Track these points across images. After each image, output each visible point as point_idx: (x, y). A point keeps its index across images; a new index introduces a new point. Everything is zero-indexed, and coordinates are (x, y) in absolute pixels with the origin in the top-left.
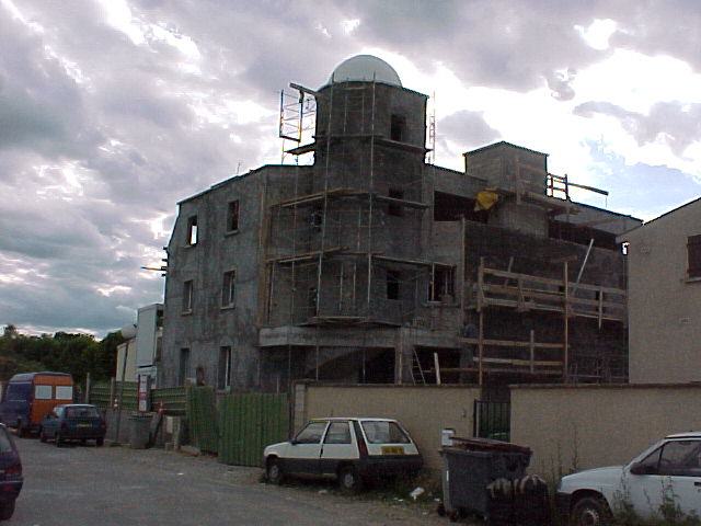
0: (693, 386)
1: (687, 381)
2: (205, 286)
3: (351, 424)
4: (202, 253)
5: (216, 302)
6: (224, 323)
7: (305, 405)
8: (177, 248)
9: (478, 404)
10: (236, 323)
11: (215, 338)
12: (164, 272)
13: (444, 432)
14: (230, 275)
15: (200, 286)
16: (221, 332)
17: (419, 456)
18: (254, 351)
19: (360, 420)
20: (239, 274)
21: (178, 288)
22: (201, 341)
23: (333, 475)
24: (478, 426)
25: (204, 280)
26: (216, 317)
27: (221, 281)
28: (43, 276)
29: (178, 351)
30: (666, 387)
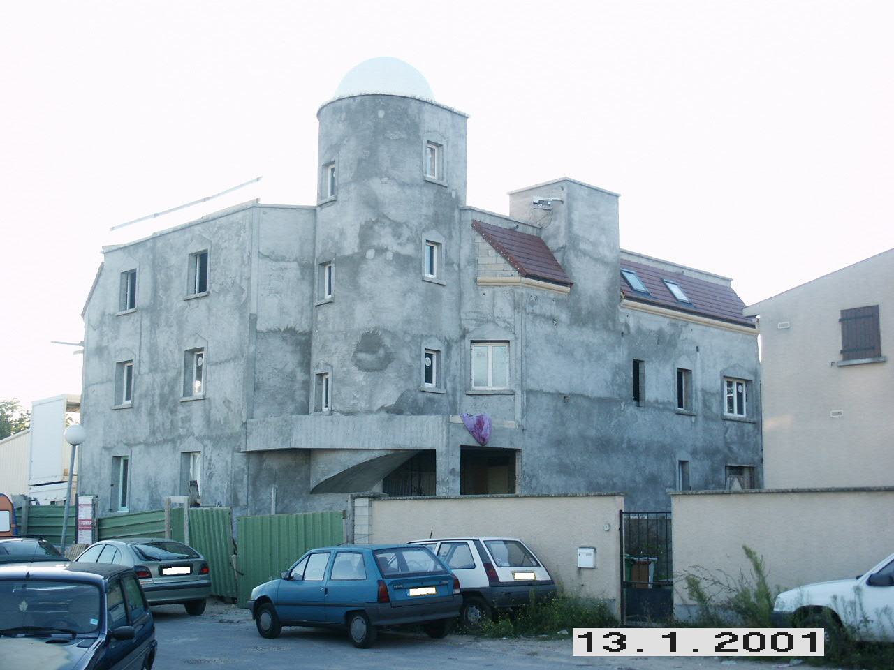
0: (889, 490)
1: (880, 484)
2: (154, 370)
3: (471, 544)
4: (146, 322)
5: (172, 392)
6: (187, 420)
7: (370, 525)
8: (103, 315)
9: (624, 517)
10: (208, 420)
11: (173, 441)
12: (82, 348)
13: (580, 550)
14: (196, 352)
15: (145, 369)
16: (182, 432)
17: (552, 582)
18: (238, 456)
19: (481, 540)
20: (211, 351)
21: (106, 369)
22: (147, 445)
23: (458, 614)
24: (297, 562)
25: (152, 360)
26: (173, 412)
27: (179, 359)
28: (661, 355)
29: (108, 460)
30: (810, 491)
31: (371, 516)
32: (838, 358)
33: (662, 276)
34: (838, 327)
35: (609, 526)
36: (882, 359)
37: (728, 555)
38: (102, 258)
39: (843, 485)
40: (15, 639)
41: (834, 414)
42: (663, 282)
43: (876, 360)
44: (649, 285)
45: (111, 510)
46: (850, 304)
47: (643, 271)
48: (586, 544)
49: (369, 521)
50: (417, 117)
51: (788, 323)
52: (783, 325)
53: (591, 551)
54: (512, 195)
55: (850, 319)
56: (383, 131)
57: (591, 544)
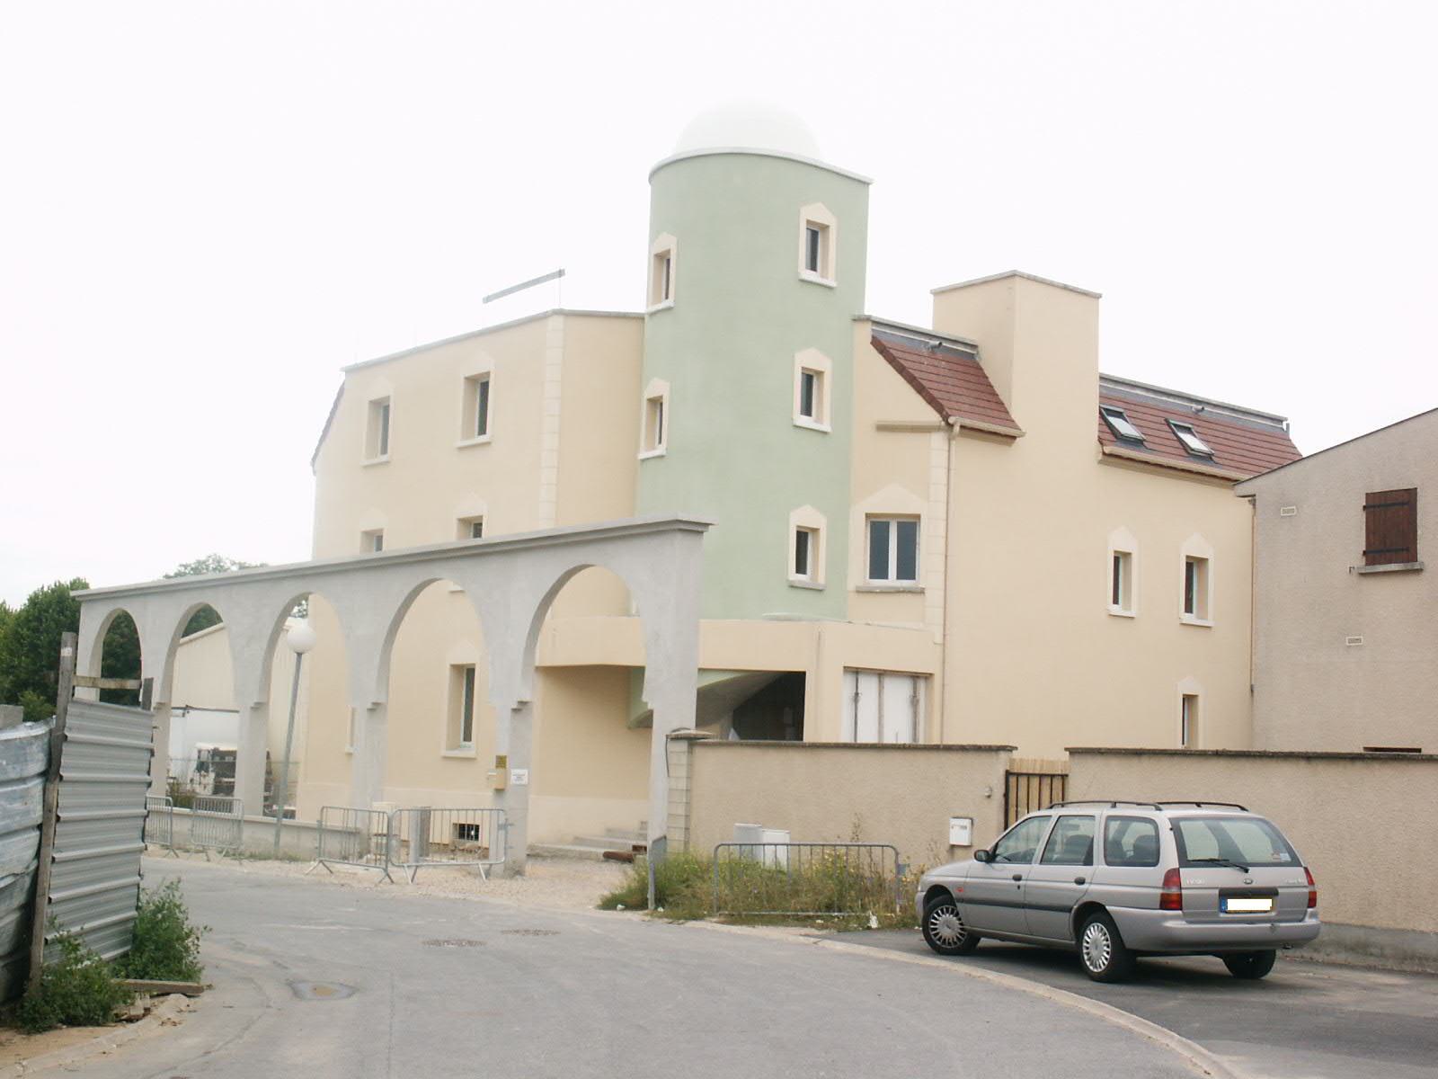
7: (689, 778)
13: (954, 822)
31: (691, 765)
32: (1359, 561)
33: (1166, 415)
34: (1361, 518)
35: (991, 790)
36: (1417, 566)
37: (987, 794)
38: (343, 377)
39: (291, 679)
40: (105, 1028)
41: (1351, 641)
42: (1168, 424)
43: (1409, 566)
44: (1145, 430)
45: (53, 859)
46: (1378, 488)
47: (1138, 408)
48: (961, 813)
49: (688, 772)
50: (486, 890)
51: (1294, 507)
52: (1289, 511)
53: (967, 822)
54: (938, 293)
55: (1379, 506)
56: (750, 215)
57: (970, 816)
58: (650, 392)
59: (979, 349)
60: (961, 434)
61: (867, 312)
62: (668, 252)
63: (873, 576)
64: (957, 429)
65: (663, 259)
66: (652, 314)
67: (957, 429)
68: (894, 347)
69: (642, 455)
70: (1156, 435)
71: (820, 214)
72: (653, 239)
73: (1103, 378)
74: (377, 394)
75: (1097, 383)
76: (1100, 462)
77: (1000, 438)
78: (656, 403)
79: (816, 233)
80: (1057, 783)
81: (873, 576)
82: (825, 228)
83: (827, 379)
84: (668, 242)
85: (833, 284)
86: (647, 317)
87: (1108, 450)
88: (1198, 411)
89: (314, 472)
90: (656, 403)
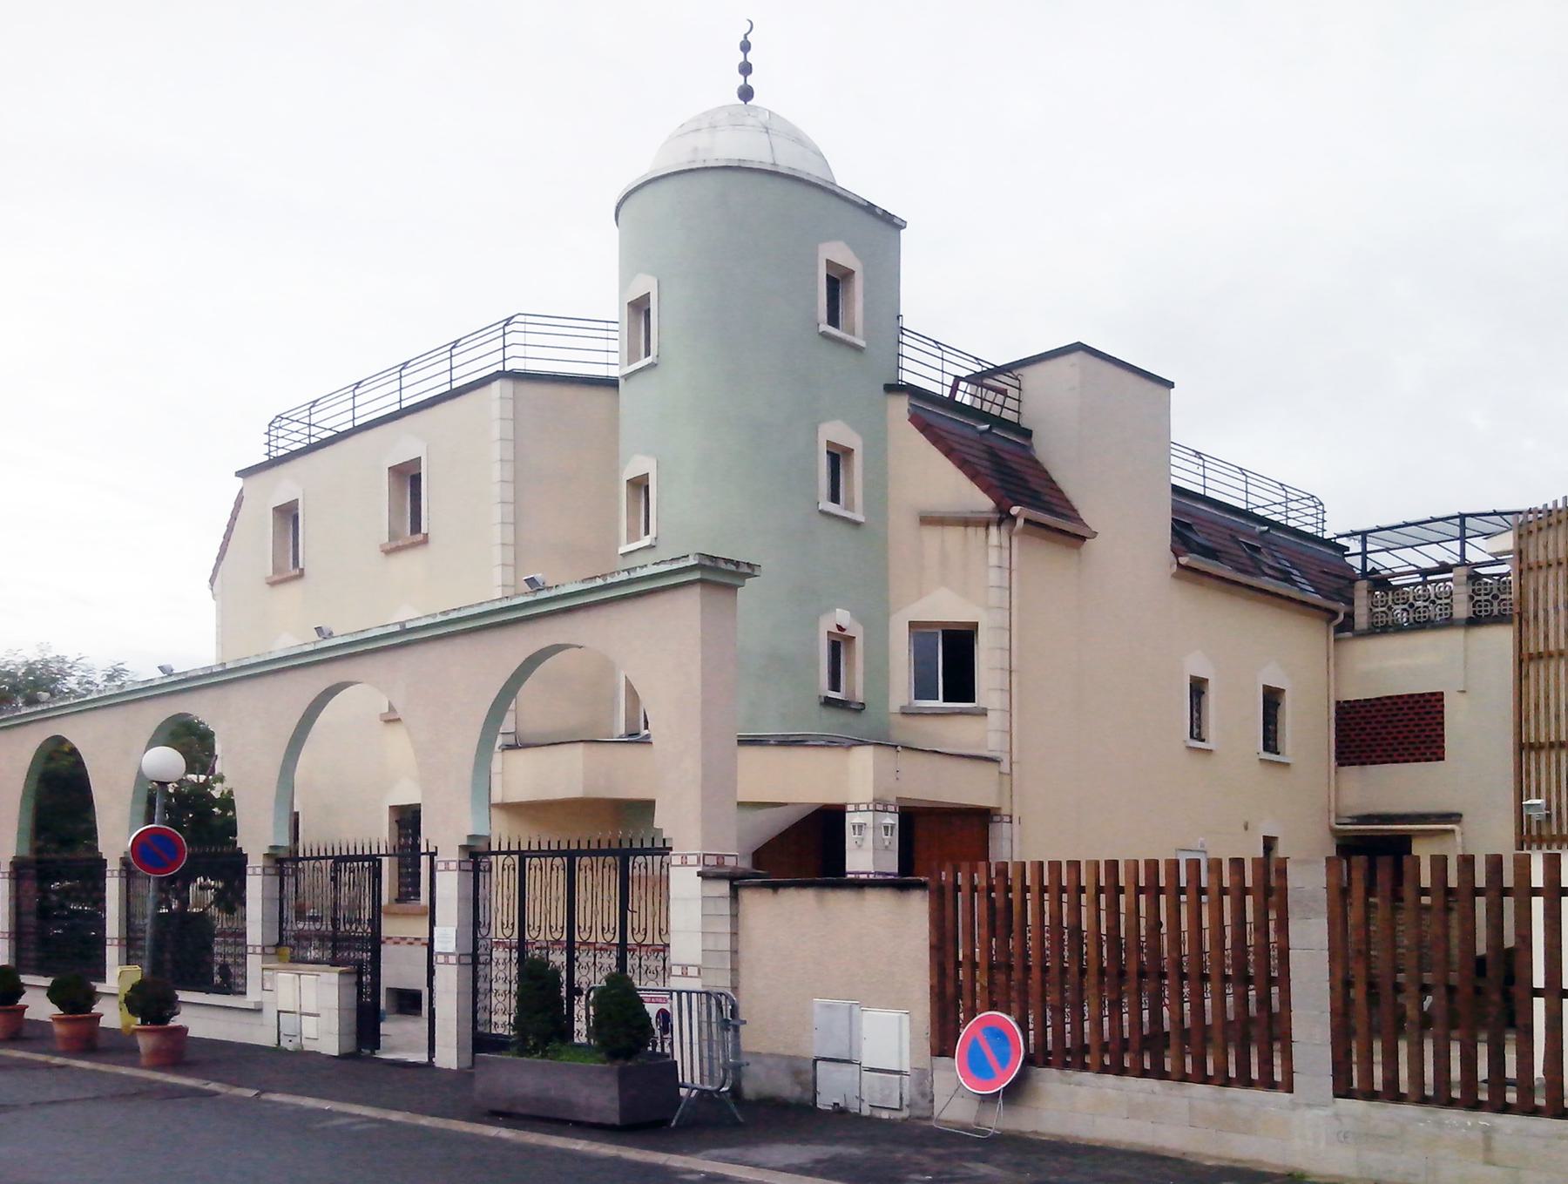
58: (631, 471)
59: (1034, 439)
60: (1024, 531)
61: (907, 378)
62: (647, 297)
63: (919, 696)
64: (1020, 522)
65: (640, 308)
66: (627, 377)
67: (1020, 522)
68: (936, 417)
69: (622, 550)
70: (1228, 548)
71: (844, 256)
72: (624, 285)
73: (1177, 490)
74: (282, 499)
75: (1168, 494)
76: (1174, 576)
77: (1067, 538)
78: (640, 485)
79: (838, 457)
80: (1384, 865)
81: (919, 696)
82: (849, 452)
83: (858, 460)
84: (645, 284)
85: (860, 518)
86: (621, 382)
87: (1183, 560)
88: (1263, 532)
89: (214, 596)
90: (640, 485)
